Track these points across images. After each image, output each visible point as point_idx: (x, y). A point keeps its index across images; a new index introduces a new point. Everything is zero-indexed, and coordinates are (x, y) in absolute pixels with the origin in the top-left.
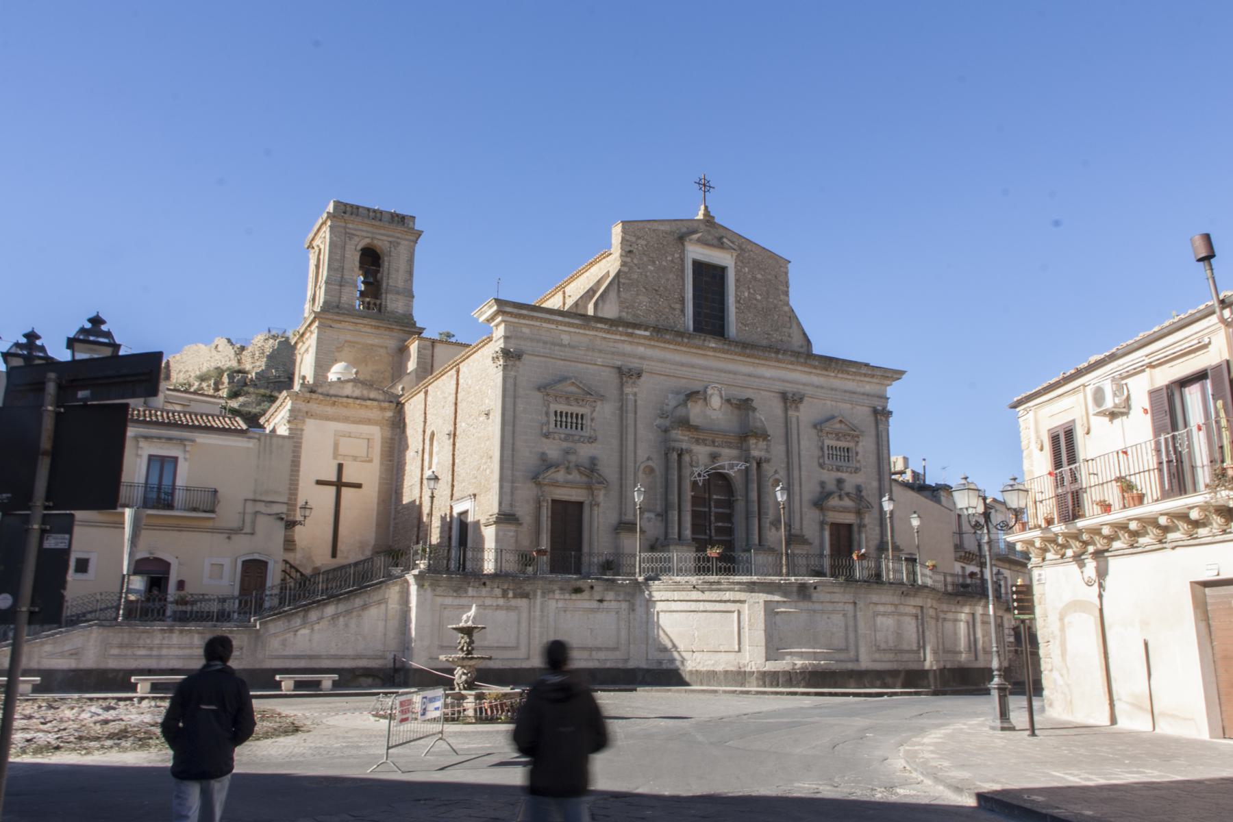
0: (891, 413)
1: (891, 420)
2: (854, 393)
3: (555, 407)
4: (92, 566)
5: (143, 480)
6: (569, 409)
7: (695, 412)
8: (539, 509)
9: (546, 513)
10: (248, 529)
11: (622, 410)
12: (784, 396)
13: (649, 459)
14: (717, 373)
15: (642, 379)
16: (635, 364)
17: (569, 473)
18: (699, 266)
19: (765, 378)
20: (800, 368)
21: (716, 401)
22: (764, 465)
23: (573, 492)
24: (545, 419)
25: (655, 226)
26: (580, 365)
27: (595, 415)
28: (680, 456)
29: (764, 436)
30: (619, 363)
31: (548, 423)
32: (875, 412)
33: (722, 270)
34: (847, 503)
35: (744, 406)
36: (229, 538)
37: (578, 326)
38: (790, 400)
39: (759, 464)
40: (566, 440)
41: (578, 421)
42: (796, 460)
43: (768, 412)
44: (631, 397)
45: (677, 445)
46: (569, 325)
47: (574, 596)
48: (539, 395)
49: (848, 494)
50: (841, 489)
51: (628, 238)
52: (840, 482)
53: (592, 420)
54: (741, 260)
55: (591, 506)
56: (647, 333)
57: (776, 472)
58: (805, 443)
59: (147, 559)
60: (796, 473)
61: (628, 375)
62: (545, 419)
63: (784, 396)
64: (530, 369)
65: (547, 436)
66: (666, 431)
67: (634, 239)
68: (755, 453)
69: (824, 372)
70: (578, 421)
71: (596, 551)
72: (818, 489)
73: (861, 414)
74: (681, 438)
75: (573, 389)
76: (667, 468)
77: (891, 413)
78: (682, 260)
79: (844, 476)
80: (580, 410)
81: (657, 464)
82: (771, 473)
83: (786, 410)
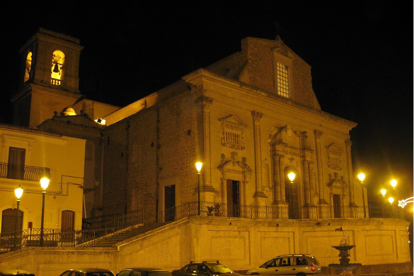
4: (328, 224)
5: (7, 161)
8: (222, 184)
9: (225, 184)
10: (64, 193)
12: (253, 113)
17: (234, 166)
23: (237, 175)
24: (222, 136)
27: (243, 135)
31: (224, 138)
34: (237, 168)
36: (55, 197)
44: (258, 127)
47: (317, 229)
49: (238, 162)
50: (234, 159)
52: (336, 174)
53: (242, 138)
55: (244, 182)
56: (265, 95)
59: (11, 209)
61: (256, 115)
63: (253, 113)
65: (224, 145)
72: (220, 159)
75: (234, 121)
79: (337, 171)
83: (316, 139)
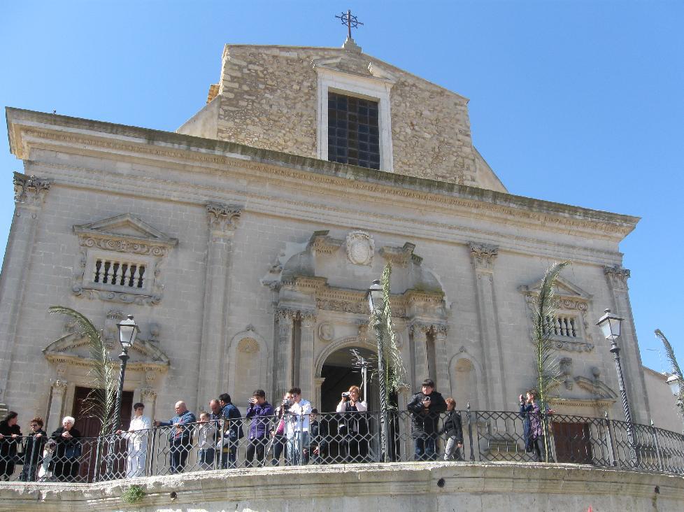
0: (627, 273)
1: (629, 281)
2: (573, 247)
3: (96, 254)
6: (122, 258)
7: (330, 267)
11: (207, 262)
13: (250, 328)
14: (366, 223)
15: (241, 219)
16: (230, 199)
18: (339, 102)
19: (441, 233)
20: (487, 212)
21: (360, 251)
22: (440, 338)
25: (276, 52)
26: (145, 202)
27: (162, 267)
28: (297, 323)
29: (436, 293)
30: (204, 199)
32: (606, 271)
33: (375, 104)
35: (407, 256)
37: (139, 149)
38: (482, 253)
39: (431, 336)
40: (110, 300)
41: (134, 277)
42: (492, 332)
43: (445, 262)
45: (293, 305)
46: (127, 146)
48: (74, 240)
51: (235, 61)
54: (399, 89)
57: (462, 350)
58: (505, 311)
60: (493, 351)
61: (221, 213)
62: (78, 269)
64: (63, 207)
66: (277, 289)
67: (244, 64)
68: (426, 320)
69: (526, 220)
70: (134, 277)
71: (651, 500)
73: (586, 275)
74: (300, 296)
76: (279, 340)
77: (627, 273)
78: (313, 88)
80: (139, 260)
81: (263, 336)
82: (456, 350)
83: (473, 266)
